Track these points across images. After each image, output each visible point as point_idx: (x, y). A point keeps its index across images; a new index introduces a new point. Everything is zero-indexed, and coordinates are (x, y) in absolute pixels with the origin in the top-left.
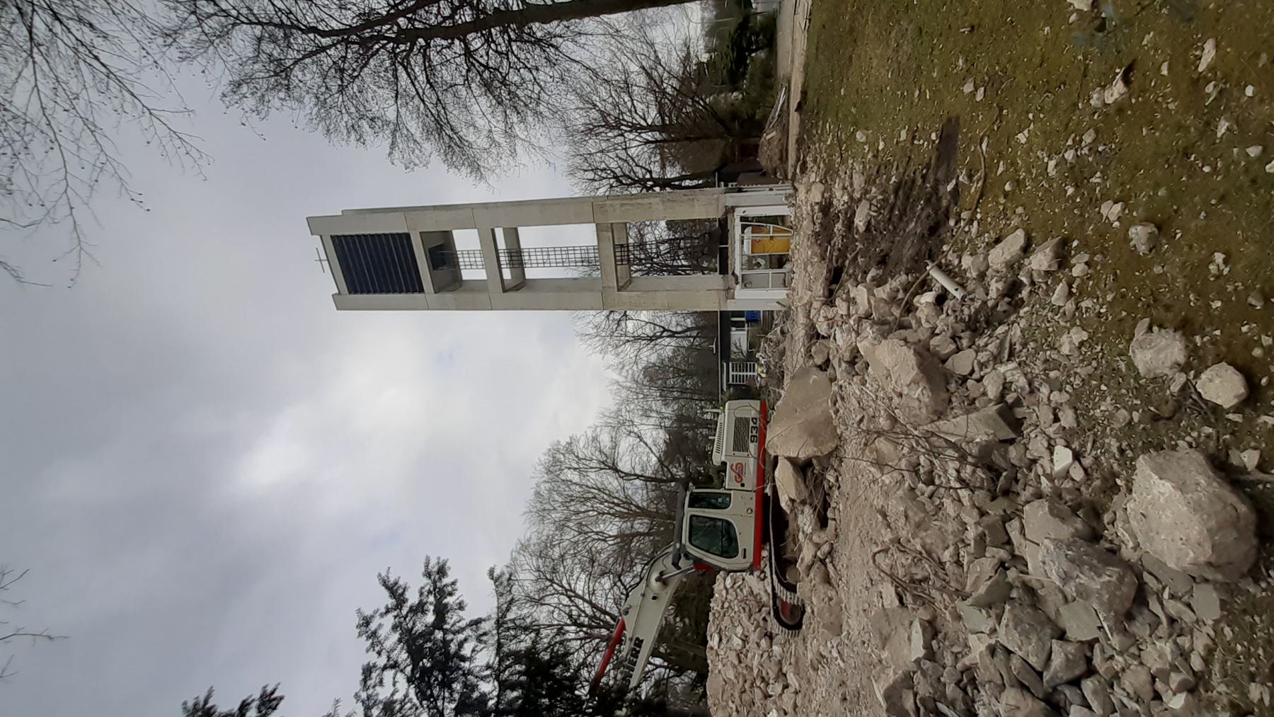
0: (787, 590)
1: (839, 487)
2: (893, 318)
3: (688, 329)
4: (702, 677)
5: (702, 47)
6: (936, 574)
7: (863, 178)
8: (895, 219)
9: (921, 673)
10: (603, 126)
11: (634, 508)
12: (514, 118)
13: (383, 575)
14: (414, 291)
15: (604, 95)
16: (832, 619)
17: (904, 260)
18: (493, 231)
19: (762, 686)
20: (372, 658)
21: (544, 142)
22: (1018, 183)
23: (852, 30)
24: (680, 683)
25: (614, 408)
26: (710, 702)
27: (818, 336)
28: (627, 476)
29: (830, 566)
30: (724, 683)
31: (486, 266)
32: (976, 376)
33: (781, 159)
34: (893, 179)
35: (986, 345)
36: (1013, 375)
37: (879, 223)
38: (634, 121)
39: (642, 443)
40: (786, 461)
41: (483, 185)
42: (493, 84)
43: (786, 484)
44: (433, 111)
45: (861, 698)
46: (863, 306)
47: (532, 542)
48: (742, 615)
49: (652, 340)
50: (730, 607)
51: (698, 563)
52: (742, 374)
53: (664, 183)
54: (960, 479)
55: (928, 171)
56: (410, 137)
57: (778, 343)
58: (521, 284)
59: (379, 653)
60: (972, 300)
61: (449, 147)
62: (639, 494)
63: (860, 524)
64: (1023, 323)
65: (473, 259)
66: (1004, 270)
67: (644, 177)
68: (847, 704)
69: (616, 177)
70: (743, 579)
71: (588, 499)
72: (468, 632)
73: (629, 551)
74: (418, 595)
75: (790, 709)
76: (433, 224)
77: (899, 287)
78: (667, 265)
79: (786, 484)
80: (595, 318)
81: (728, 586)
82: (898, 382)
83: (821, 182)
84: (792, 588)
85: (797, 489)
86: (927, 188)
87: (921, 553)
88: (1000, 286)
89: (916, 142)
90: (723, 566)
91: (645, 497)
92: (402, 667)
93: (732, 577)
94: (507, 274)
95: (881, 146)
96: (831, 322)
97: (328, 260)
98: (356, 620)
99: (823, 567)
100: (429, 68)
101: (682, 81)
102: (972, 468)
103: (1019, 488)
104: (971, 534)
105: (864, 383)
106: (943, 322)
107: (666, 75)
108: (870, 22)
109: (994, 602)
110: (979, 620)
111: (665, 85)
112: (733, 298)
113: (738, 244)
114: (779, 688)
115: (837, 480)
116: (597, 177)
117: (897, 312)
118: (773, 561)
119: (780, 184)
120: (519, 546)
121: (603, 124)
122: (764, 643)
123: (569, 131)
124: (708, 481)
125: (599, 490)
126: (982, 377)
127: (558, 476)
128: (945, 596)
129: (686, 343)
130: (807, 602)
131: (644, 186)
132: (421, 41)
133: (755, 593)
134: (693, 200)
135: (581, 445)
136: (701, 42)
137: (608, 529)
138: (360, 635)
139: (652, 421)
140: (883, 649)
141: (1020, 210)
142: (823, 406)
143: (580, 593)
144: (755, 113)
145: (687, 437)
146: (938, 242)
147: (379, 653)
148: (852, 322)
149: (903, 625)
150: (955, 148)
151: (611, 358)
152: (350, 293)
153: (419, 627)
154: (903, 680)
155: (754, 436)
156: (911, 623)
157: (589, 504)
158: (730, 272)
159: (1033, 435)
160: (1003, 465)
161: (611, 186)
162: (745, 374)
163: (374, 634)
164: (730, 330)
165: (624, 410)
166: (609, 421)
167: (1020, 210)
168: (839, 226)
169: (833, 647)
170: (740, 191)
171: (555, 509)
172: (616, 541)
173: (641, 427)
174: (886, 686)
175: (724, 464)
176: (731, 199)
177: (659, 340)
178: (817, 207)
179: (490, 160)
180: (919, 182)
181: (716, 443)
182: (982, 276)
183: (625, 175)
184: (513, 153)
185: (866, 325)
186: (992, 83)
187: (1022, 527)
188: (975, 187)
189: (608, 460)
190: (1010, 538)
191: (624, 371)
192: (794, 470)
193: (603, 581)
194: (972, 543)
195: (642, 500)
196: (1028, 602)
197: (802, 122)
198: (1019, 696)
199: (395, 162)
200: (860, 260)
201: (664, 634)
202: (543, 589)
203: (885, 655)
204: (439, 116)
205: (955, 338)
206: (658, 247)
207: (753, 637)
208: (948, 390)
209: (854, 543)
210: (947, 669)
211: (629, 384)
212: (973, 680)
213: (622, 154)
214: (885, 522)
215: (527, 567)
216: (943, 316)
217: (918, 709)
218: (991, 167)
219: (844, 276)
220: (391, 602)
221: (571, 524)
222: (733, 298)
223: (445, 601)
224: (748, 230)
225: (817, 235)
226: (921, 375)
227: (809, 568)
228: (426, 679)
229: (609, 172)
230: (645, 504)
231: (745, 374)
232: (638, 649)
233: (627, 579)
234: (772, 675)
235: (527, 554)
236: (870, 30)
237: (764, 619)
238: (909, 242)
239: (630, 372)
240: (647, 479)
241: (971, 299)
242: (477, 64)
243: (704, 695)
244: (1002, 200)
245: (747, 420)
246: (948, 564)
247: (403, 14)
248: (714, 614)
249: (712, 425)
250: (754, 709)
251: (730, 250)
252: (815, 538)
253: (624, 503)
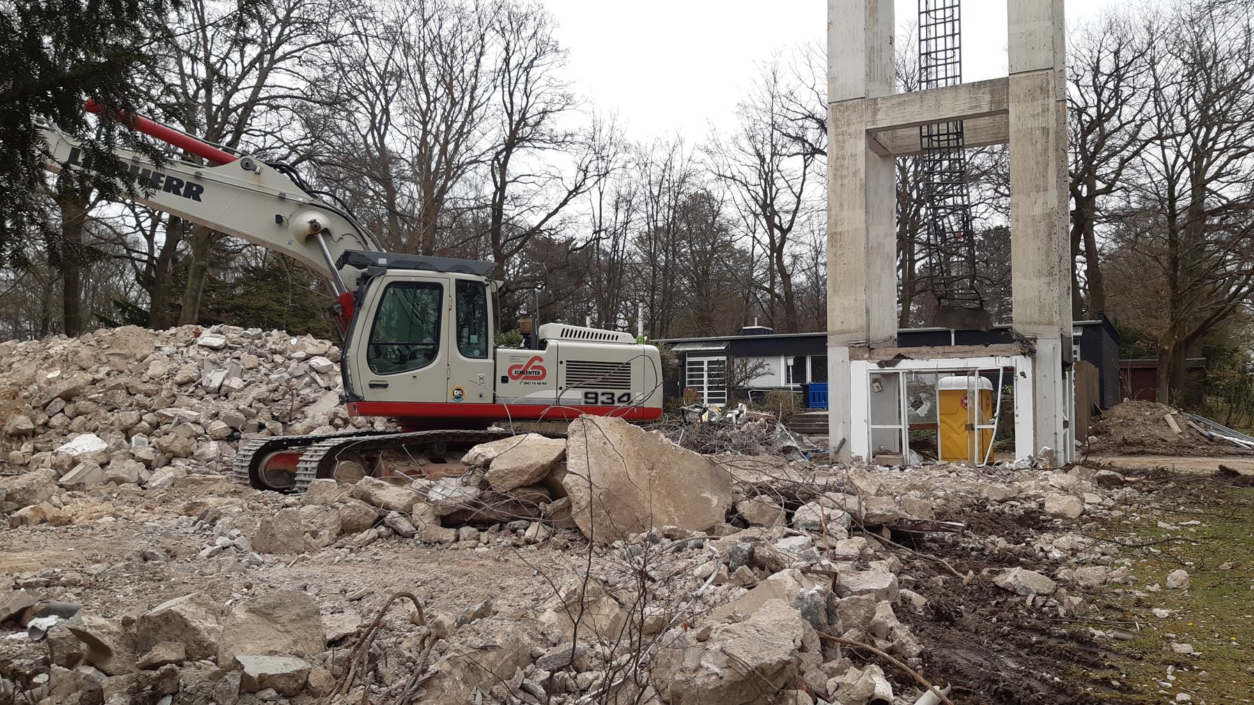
2: (841, 630)
7: (1095, 582)
8: (1021, 636)
9: (215, 673)
11: (440, 182)
16: (280, 537)
17: (945, 652)
19: (143, 423)
24: (128, 284)
25: (631, 139)
27: (792, 506)
28: (500, 167)
30: (138, 357)
33: (1125, 442)
34: (1099, 633)
37: (1011, 609)
38: (1215, 154)
39: (565, 194)
40: (556, 454)
46: (857, 581)
48: (264, 388)
49: (764, 206)
50: (276, 366)
51: (353, 302)
52: (705, 379)
53: (1083, 219)
55: (1115, 688)
57: (768, 443)
63: (456, 580)
67: (1098, 178)
68: (137, 561)
69: (1101, 118)
70: (328, 389)
71: (449, 87)
75: (110, 472)
77: (895, 643)
81: (313, 362)
82: (727, 635)
83: (1084, 512)
84: (325, 469)
85: (508, 472)
86: (1085, 687)
90: (352, 352)
91: (460, 204)
93: (330, 368)
95: (1161, 612)
96: (817, 529)
114: (145, 452)
115: (528, 542)
116: (1102, 79)
117: (850, 636)
119: (1075, 442)
121: (1213, 90)
122: (219, 426)
125: (470, 112)
127: (491, 25)
129: (758, 273)
130: (304, 495)
131: (1078, 180)
133: (305, 409)
134: (1051, 274)
137: (396, 133)
139: (609, 213)
140: (251, 611)
143: (269, 81)
144: (1218, 395)
145: (580, 282)
154: (199, 643)
155: (596, 398)
156: (299, 656)
157: (441, 91)
158: (903, 350)
161: (1081, 111)
162: (705, 385)
164: (786, 355)
165: (627, 157)
166: (605, 131)
168: (1002, 543)
169: (232, 538)
170: (1066, 366)
171: (425, 22)
172: (373, 148)
173: (595, 191)
175: (542, 345)
176: (1050, 349)
177: (764, 222)
178: (1033, 505)
180: (1096, 675)
181: (579, 328)
183: (1104, 136)
189: (528, 129)
191: (704, 155)
192: (543, 466)
193: (297, 125)
195: (455, 200)
197: (1197, 479)
200: (940, 579)
206: (954, 209)
209: (419, 570)
213: (1148, 131)
214: (469, 616)
217: (155, 666)
219: (908, 552)
222: (852, 357)
224: (986, 383)
225: (981, 506)
227: (366, 498)
229: (1112, 105)
230: (448, 205)
232: (182, 190)
234: (165, 441)
237: (261, 427)
238: (979, 659)
239: (701, 167)
240: (497, 208)
243: (112, 324)
245: (626, 384)
250: (102, 411)
251: (947, 348)
252: (420, 507)
253: (449, 163)
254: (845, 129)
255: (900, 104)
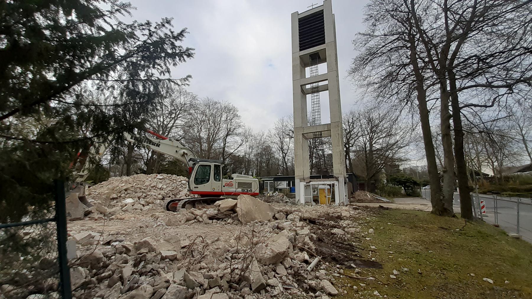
0: (183, 205)
1: (226, 224)
3: (286, 164)
4: (144, 172)
5: (406, 167)
6: (195, 260)
8: (337, 244)
10: (372, 125)
11: (212, 143)
12: (376, 86)
13: (187, 30)
14: (300, 47)
15: (385, 126)
17: (321, 248)
18: (327, 80)
20: (154, 25)
21: (365, 100)
22: (357, 292)
23: (416, 227)
24: (142, 164)
25: (253, 134)
26: (135, 175)
27: (287, 215)
28: (225, 140)
29: (194, 221)
31: (311, 77)
32: (276, 275)
33: (359, 200)
34: (354, 243)
35: (289, 279)
36: (278, 289)
41: (347, 74)
42: (391, 77)
43: (226, 203)
44: (379, 51)
45: (142, 234)
46: (300, 232)
47: (196, 101)
49: (281, 149)
51: (192, 169)
53: (347, 152)
54: (234, 269)
56: (367, 42)
58: (304, 93)
59: (156, 28)
60: (307, 274)
61: (364, 59)
62: (218, 145)
64: (299, 293)
65: (314, 72)
66: (320, 286)
68: (139, 228)
69: (350, 132)
71: (215, 124)
72: (164, 67)
73: (194, 142)
74: (179, 45)
75: (134, 207)
76: (329, 54)
78: (313, 154)
79: (226, 203)
80: (291, 125)
81: (182, 182)
83: (350, 215)
84: (183, 206)
87: (203, 254)
88: (314, 285)
89: (370, 252)
92: (150, 38)
94: (308, 87)
96: (292, 220)
97: (313, 9)
98: (169, 18)
99: (193, 218)
100: (397, 49)
101: (392, 158)
102: (239, 274)
103: (232, 291)
104: (212, 273)
105: (270, 232)
106: (297, 263)
107: (394, 151)
108: (420, 234)
109: (186, 281)
110: (179, 276)
111: (389, 151)
112: (300, 181)
113: (322, 183)
114: (143, 202)
115: (228, 223)
116: (350, 124)
117: (300, 245)
118: (193, 199)
120: (194, 96)
122: (160, 196)
123: (369, 111)
124: (225, 174)
125: (218, 129)
126: (276, 278)
127: (224, 111)
128: (187, 264)
131: (346, 144)
132: (409, 45)
135: (237, 121)
136: (408, 166)
138: (163, 19)
139: (248, 150)
140: (164, 240)
141: (346, 292)
142: (258, 217)
143: (176, 122)
145: (241, 164)
146: (329, 261)
147: (156, 28)
148: (294, 228)
149: (174, 248)
150: (369, 267)
151: (273, 132)
152: (299, 19)
153: (166, 46)
154: (152, 248)
156: (175, 251)
158: (311, 180)
159: (254, 297)
160: (241, 286)
161: (346, 130)
162: (269, 187)
163: (164, 26)
167: (346, 292)
168: (333, 223)
170: (345, 183)
173: (245, 145)
174: (150, 242)
175: (232, 179)
176: (341, 179)
178: (339, 214)
179: (358, 77)
180: (354, 253)
182: (317, 278)
183: (351, 135)
184: (361, 86)
185: (294, 233)
186: (398, 282)
187: (217, 293)
188: (354, 275)
190: (212, 288)
192: (232, 206)
193: (182, 131)
194: (209, 274)
195: (215, 147)
196: (187, 295)
197: (374, 208)
198: (150, 292)
199: (356, 36)
200: (319, 231)
201: (161, 156)
202: (177, 106)
203: (162, 241)
204: (377, 54)
205: (291, 267)
207: (162, 192)
208: (270, 264)
210: (158, 265)
211: (263, 140)
212: (154, 275)
215: (186, 99)
216: (299, 263)
217: (141, 254)
218: (363, 281)
219: (312, 225)
220: (175, 34)
221: (204, 117)
222: (300, 181)
223: (177, 57)
224: (329, 187)
226: (276, 254)
227: (192, 213)
228: (145, 50)
230: (213, 148)
231: (269, 187)
233: (183, 141)
234: (148, 200)
235: (191, 99)
236: (417, 234)
237: (170, 196)
238: (328, 250)
240: (224, 148)
241: (307, 273)
242: (399, 70)
244: (349, 285)
246: (200, 265)
247: (421, 36)
248: (170, 176)
249: (247, 173)
250: (134, 193)
253: (214, 139)
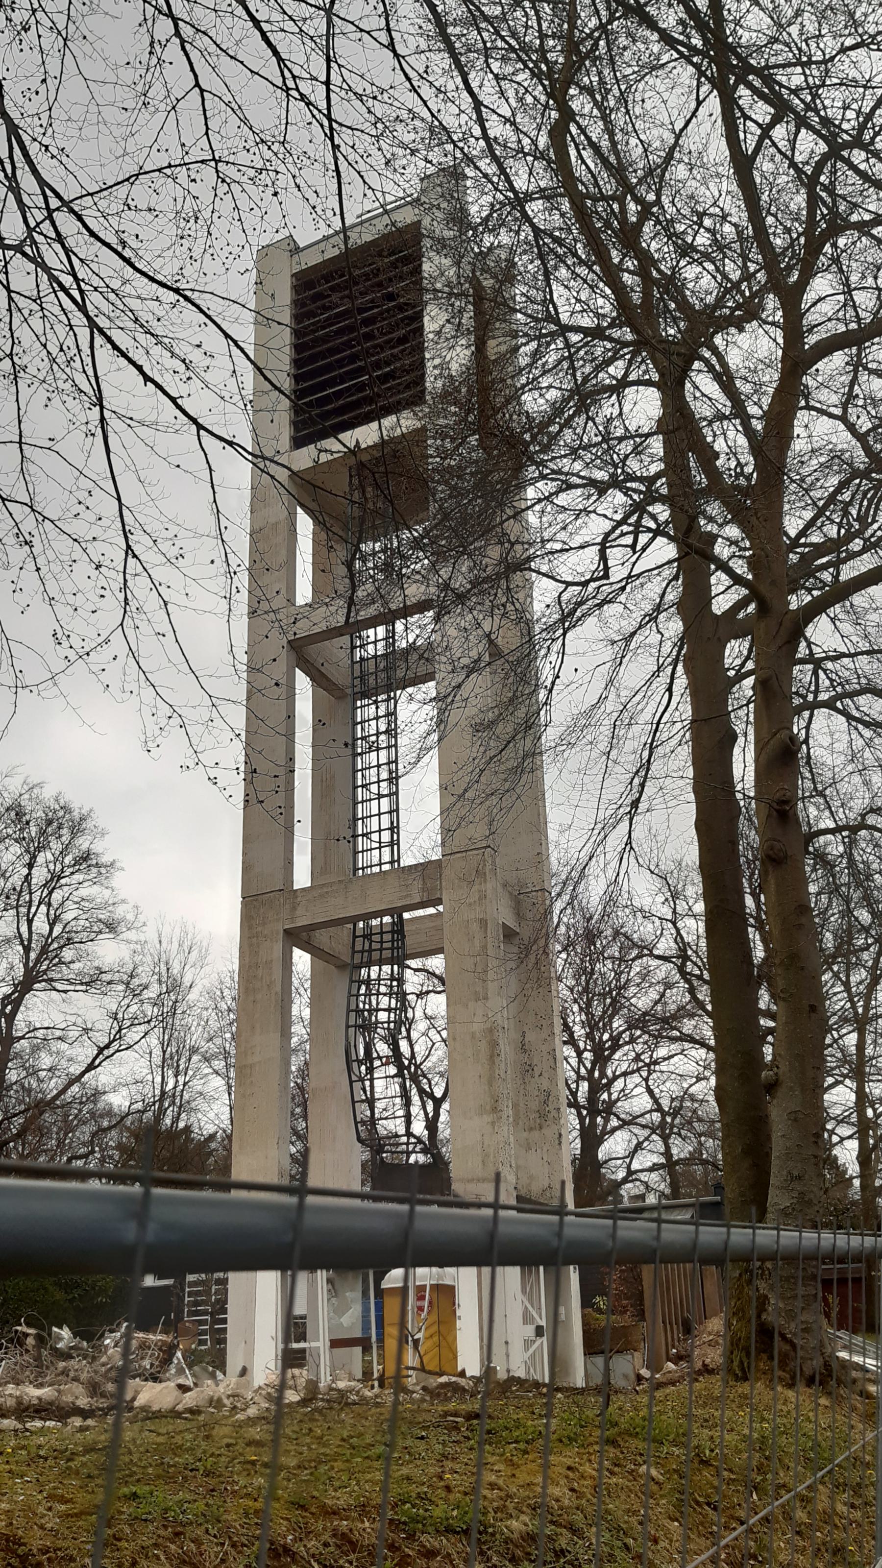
254: (259, 929)
255: (321, 896)
